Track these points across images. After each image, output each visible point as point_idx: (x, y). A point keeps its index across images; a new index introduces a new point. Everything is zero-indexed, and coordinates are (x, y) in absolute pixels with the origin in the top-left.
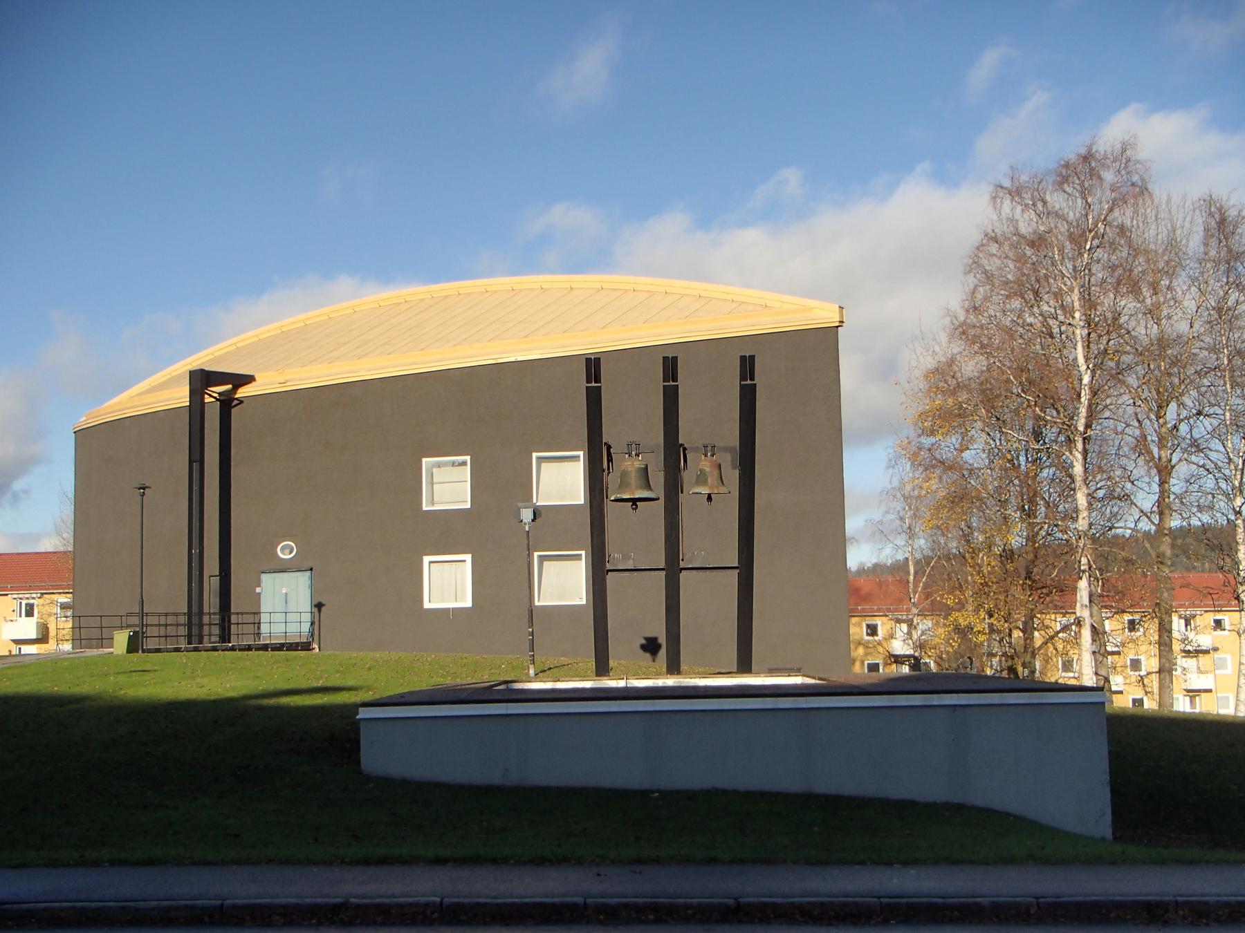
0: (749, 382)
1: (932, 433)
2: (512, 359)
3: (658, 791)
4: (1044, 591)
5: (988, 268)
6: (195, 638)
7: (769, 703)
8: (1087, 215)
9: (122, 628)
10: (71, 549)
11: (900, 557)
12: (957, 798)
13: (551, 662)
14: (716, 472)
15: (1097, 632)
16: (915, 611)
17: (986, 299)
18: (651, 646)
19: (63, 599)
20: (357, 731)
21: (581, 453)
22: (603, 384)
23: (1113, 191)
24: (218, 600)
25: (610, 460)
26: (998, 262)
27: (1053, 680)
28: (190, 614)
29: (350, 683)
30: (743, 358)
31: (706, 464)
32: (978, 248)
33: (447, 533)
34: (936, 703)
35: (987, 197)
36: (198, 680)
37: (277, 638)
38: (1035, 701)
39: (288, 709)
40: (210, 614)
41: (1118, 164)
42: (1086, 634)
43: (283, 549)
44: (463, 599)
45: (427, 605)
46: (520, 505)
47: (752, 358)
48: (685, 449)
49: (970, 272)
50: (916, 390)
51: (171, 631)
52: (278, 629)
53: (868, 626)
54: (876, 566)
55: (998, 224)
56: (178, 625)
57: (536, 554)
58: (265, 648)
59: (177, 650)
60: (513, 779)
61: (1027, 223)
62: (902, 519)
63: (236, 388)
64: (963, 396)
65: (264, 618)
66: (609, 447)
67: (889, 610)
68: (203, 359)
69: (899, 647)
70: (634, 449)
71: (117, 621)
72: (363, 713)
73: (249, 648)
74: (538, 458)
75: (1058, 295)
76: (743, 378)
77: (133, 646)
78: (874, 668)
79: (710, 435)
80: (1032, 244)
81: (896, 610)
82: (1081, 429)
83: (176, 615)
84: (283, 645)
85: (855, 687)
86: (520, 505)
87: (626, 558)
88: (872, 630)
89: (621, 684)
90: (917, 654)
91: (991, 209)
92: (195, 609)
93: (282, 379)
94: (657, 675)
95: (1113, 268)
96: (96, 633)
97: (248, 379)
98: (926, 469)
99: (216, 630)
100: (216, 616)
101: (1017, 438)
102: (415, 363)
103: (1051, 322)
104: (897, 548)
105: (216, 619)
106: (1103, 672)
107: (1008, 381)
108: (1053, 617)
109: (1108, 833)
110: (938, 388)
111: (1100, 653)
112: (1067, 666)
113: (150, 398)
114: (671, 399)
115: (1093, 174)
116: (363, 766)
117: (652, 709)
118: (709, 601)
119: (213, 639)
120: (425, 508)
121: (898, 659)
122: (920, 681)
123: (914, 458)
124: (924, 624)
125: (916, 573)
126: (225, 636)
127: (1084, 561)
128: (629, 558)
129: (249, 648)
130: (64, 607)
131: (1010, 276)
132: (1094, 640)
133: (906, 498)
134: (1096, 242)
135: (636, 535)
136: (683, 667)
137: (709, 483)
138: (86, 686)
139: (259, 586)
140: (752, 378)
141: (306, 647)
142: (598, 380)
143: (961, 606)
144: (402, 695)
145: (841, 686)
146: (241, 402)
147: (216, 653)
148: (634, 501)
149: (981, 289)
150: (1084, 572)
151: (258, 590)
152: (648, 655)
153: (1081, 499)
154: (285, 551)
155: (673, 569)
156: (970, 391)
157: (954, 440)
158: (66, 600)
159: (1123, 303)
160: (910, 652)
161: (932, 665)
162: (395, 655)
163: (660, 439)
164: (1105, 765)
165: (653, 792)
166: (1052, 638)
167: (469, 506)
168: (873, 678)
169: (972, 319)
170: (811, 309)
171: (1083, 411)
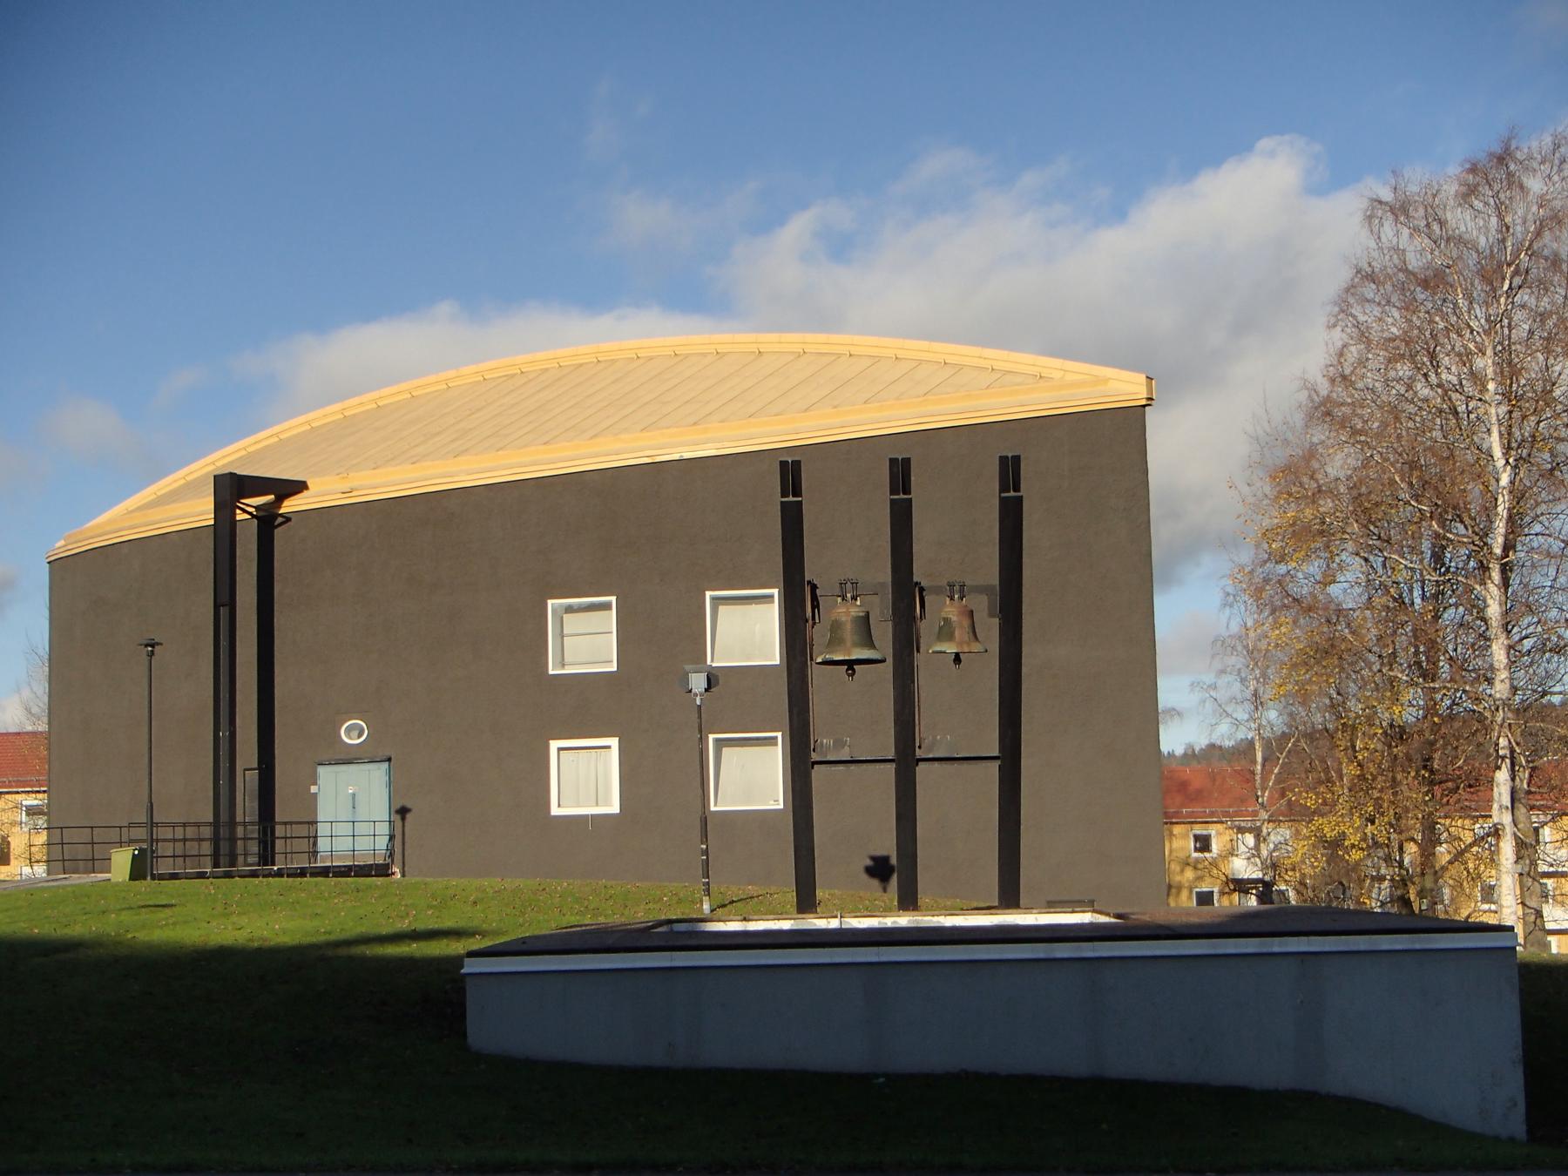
0: (1012, 494)
1: (1282, 559)
2: (676, 457)
3: (884, 1075)
4: (1450, 784)
5: (1362, 318)
6: (224, 858)
8: (1504, 240)
9: (121, 844)
10: (43, 727)
11: (1243, 734)
13: (734, 892)
14: (966, 623)
15: (1526, 848)
16: (1264, 815)
17: (1362, 362)
18: (879, 869)
19: (31, 801)
20: (462, 991)
21: (775, 592)
22: (805, 498)
23: (1541, 206)
24: (256, 804)
25: (815, 605)
26: (1377, 311)
27: (1464, 913)
28: (216, 824)
29: (448, 923)
30: (1003, 460)
31: (951, 611)
32: (1347, 290)
33: (582, 707)
35: (1358, 218)
36: (234, 918)
37: (340, 858)
38: (1418, 946)
39: (364, 960)
40: (244, 824)
41: (1547, 165)
42: (1507, 848)
43: (348, 730)
44: (608, 803)
45: (555, 811)
46: (688, 667)
47: (1017, 459)
48: (922, 590)
49: (1334, 326)
50: (1259, 494)
51: (192, 848)
52: (343, 845)
53: (1197, 838)
54: (1212, 746)
55: (1375, 254)
56: (175, 840)
57: (711, 737)
58: (325, 872)
59: (202, 876)
61: (1418, 253)
62: (1243, 681)
63: (280, 499)
64: (1327, 505)
65: (323, 829)
66: (814, 587)
67: (1226, 814)
68: (232, 456)
69: (1242, 867)
70: (849, 589)
71: (114, 835)
72: (471, 966)
73: (302, 873)
74: (713, 599)
75: (1465, 358)
76: (1004, 488)
77: (139, 870)
78: (1205, 899)
79: (954, 569)
80: (1425, 284)
81: (1237, 814)
82: (1498, 551)
83: (198, 825)
84: (350, 868)
85: (1161, 926)
86: (688, 667)
87: (839, 744)
88: (1203, 843)
89: (834, 924)
90: (1267, 878)
91: (1365, 232)
92: (224, 817)
94: (886, 911)
95: (1543, 316)
96: (83, 852)
97: (298, 487)
98: (1273, 612)
99: (254, 848)
100: (254, 829)
101: (1409, 567)
102: (534, 463)
103: (1455, 396)
104: (1237, 723)
105: (254, 831)
106: (1533, 903)
107: (1392, 482)
108: (1459, 823)
109: (1516, 1125)
110: (1290, 495)
111: (1530, 876)
112: (1489, 893)
113: (156, 514)
114: (902, 518)
115: (1512, 181)
116: (470, 1040)
117: (874, 959)
118: (958, 804)
119: (250, 860)
120: (551, 672)
121: (1241, 886)
122: (1272, 920)
123: (1258, 592)
124: (1279, 835)
125: (1265, 760)
126: (267, 857)
127: (1503, 742)
128: (843, 744)
129: (302, 873)
130: (31, 811)
131: (1394, 330)
132: (1519, 858)
133: (1250, 653)
134: (1517, 281)
135: (854, 714)
136: (923, 899)
137: (956, 640)
138: (80, 928)
139: (315, 783)
140: (1017, 489)
141: (383, 871)
142: (797, 493)
143: (1327, 808)
144: (524, 941)
145: (1147, 926)
146: (288, 520)
147: (256, 881)
148: (850, 664)
149: (1353, 349)
150: (1503, 758)
151: (314, 789)
152: (875, 883)
153: (1499, 654)
154: (352, 732)
155: (906, 760)
156: (1336, 496)
157: (1315, 568)
158: (35, 802)
159: (1558, 368)
160: (1258, 875)
161: (1292, 894)
162: (510, 883)
163: (885, 576)
164: (1516, 1037)
165: (877, 1076)
166: (1461, 853)
167: (615, 669)
168: (1204, 915)
169: (1340, 393)
170: (1106, 380)
171: (1500, 527)
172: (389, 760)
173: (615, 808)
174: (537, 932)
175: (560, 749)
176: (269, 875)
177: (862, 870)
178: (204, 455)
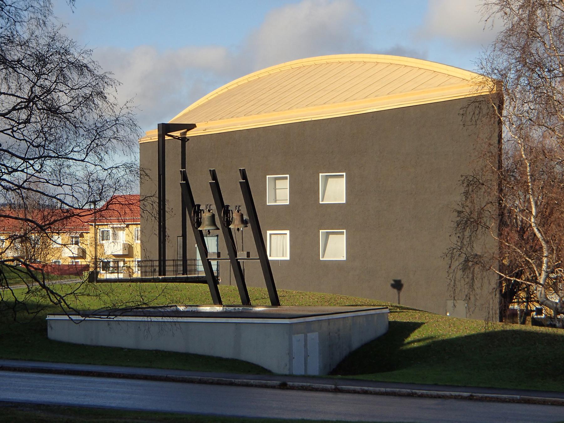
7: (301, 320)
12: (236, 358)
33: (334, 217)
34: (230, 321)
60: (94, 343)
93: (206, 127)
97: (191, 127)
146: (188, 140)
152: (395, 291)
172: (217, 236)
173: (288, 258)
174: (210, 295)
175: (271, 235)
176: (164, 280)
177: (390, 285)
178: (265, 68)
